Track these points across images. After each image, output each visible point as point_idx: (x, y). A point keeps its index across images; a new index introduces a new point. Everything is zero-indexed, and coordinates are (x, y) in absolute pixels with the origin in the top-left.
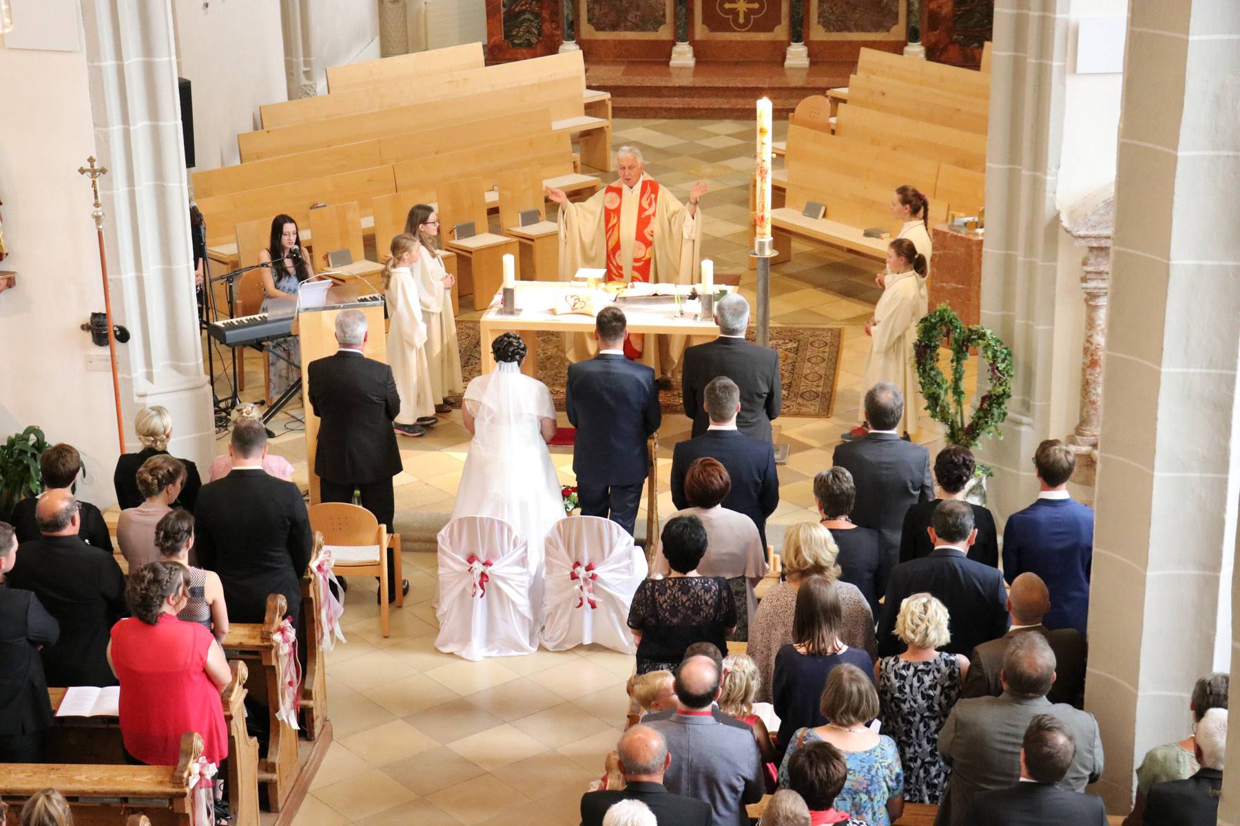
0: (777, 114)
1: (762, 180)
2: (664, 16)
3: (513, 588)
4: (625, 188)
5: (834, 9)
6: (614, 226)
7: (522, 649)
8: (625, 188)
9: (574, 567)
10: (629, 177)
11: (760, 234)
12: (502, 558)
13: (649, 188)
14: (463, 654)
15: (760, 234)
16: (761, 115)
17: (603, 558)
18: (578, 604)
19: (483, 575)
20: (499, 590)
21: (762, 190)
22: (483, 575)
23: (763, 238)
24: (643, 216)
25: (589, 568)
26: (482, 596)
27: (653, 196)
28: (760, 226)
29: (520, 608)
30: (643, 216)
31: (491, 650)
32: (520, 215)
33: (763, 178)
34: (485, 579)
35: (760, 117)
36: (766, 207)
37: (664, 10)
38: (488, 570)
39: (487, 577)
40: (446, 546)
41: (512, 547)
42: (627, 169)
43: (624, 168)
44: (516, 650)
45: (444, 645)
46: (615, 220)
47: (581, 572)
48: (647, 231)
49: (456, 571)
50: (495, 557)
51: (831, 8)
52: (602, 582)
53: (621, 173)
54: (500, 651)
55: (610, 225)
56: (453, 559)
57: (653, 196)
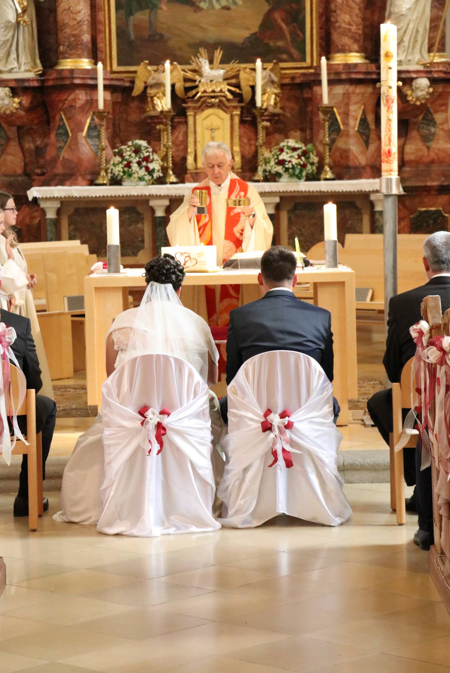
0: (362, 122)
1: (388, 111)
2: (143, 241)
3: (193, 446)
4: (212, 185)
5: (303, 230)
6: (205, 225)
7: (201, 523)
8: (212, 185)
9: (266, 415)
10: (218, 176)
11: (387, 171)
12: (180, 409)
13: (238, 186)
14: (135, 532)
15: (387, 171)
16: (386, 36)
17: (300, 406)
18: (271, 462)
19: (160, 427)
20: (178, 450)
21: (389, 120)
22: (160, 427)
23: (390, 174)
24: (232, 214)
25: (283, 415)
26: (159, 452)
27: (242, 194)
28: (387, 162)
29: (200, 472)
30: (232, 214)
31: (168, 528)
32: (66, 299)
33: (389, 108)
34: (162, 432)
35: (385, 40)
36: (392, 140)
37: (143, 236)
38: (166, 421)
39: (164, 429)
40: (112, 398)
41: (192, 396)
42: (216, 167)
43: (213, 166)
44: (197, 526)
45: (110, 524)
46: (207, 219)
47: (275, 419)
48: (236, 230)
49: (127, 429)
50: (173, 407)
51: (300, 230)
52: (298, 433)
53: (209, 172)
54: (178, 528)
55: (202, 223)
56: (122, 416)
57: (242, 194)
